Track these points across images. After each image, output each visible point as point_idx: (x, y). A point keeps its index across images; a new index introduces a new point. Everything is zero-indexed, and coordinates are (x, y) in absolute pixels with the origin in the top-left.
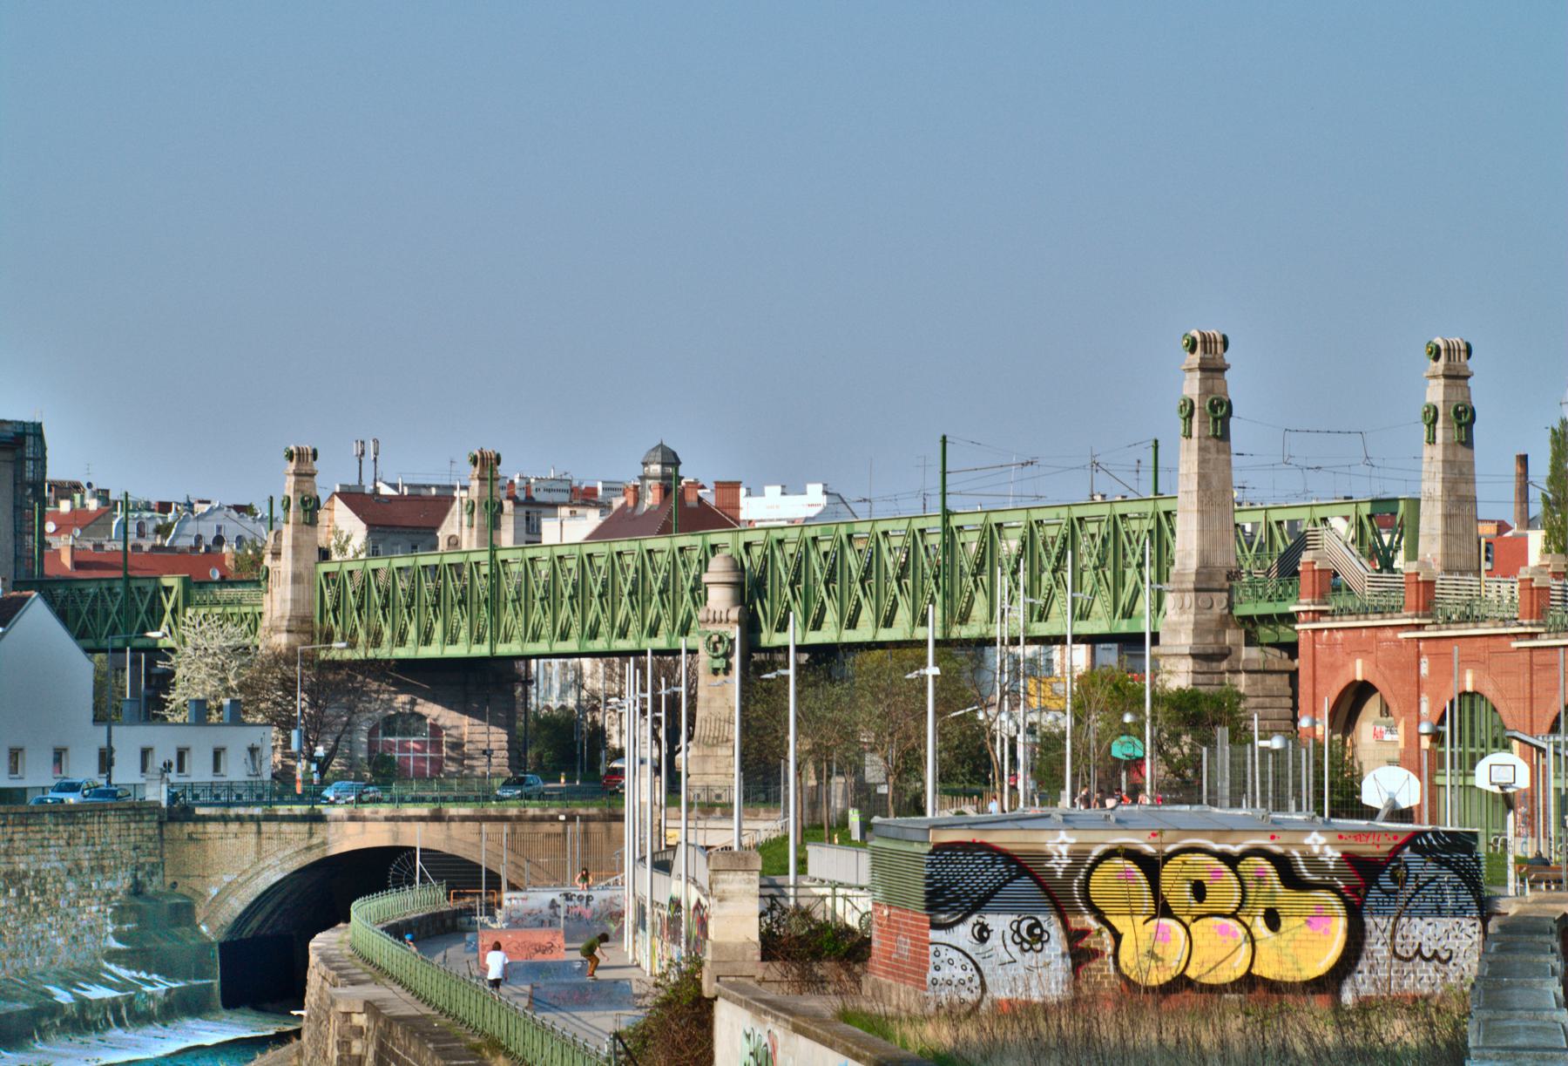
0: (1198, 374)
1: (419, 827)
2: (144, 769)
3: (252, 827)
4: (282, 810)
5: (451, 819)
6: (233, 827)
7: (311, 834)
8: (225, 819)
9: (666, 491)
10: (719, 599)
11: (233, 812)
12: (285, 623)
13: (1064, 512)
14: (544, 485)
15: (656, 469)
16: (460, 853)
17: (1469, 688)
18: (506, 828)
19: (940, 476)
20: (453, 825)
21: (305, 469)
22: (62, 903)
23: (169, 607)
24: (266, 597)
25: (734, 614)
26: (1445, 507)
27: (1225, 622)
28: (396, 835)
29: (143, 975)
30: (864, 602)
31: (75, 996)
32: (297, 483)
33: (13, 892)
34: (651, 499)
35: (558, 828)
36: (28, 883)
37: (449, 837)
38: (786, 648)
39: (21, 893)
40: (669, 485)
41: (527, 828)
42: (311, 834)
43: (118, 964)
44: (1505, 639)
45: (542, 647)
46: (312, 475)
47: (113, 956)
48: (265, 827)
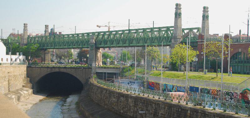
1: (62, 69)
3: (39, 69)
18: (75, 69)
33: (15, 78)
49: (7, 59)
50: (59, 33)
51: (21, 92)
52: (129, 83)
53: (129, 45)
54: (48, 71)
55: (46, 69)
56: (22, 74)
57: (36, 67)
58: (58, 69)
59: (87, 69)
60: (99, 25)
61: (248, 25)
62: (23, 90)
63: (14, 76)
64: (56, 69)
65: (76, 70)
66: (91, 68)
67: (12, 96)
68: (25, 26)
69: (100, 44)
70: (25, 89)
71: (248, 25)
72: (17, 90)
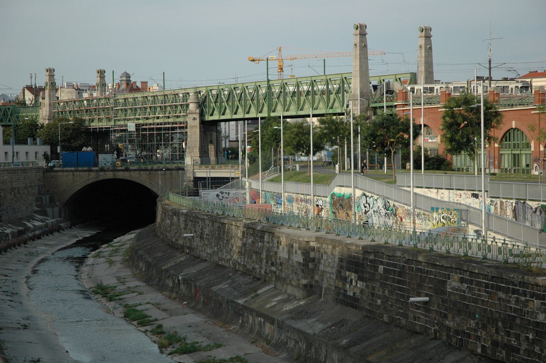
0: (359, 36)
1: (122, 173)
2: (36, 157)
3: (72, 173)
4: (80, 169)
5: (131, 170)
6: (66, 174)
7: (89, 175)
8: (63, 171)
9: (128, 84)
10: (192, 107)
11: (65, 169)
12: (47, 117)
13: (309, 79)
14: (82, 85)
15: (125, 78)
16: (134, 180)
17: (514, 127)
18: (148, 173)
19: (266, 70)
20: (132, 172)
21: (51, 74)
22: (24, 196)
23: (9, 114)
24: (40, 111)
25: (198, 111)
26: (425, 75)
27: (368, 109)
28: (115, 175)
29: (45, 217)
30: (252, 105)
31: (33, 225)
32: (49, 78)
33: (13, 193)
34: (124, 86)
35: (163, 172)
36: (16, 191)
37: (131, 176)
38: (280, 117)
39: (15, 194)
40: (128, 82)
41: (154, 173)
42: (89, 175)
43: (38, 214)
44: (529, 111)
45: (227, 116)
46: (54, 76)
47: (36, 212)
48: (75, 173)
49: (6, 153)
50: (142, 82)
51: (27, 223)
52: (220, 194)
53: (269, 114)
54: (91, 177)
55: (87, 173)
56: (31, 186)
57: (63, 171)
58: (111, 173)
59: (174, 172)
60: (255, 57)
61: (490, 69)
62: (34, 219)
63: (13, 189)
64: (107, 173)
65: (150, 174)
66: (183, 169)
67: (6, 230)
68: (51, 72)
69: (212, 115)
70: (39, 217)
71: (490, 69)
72: (21, 219)
